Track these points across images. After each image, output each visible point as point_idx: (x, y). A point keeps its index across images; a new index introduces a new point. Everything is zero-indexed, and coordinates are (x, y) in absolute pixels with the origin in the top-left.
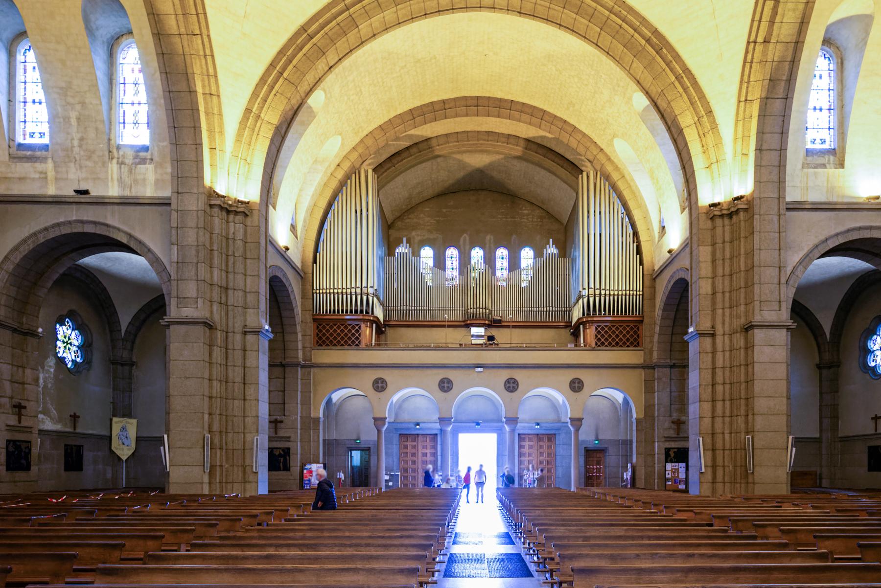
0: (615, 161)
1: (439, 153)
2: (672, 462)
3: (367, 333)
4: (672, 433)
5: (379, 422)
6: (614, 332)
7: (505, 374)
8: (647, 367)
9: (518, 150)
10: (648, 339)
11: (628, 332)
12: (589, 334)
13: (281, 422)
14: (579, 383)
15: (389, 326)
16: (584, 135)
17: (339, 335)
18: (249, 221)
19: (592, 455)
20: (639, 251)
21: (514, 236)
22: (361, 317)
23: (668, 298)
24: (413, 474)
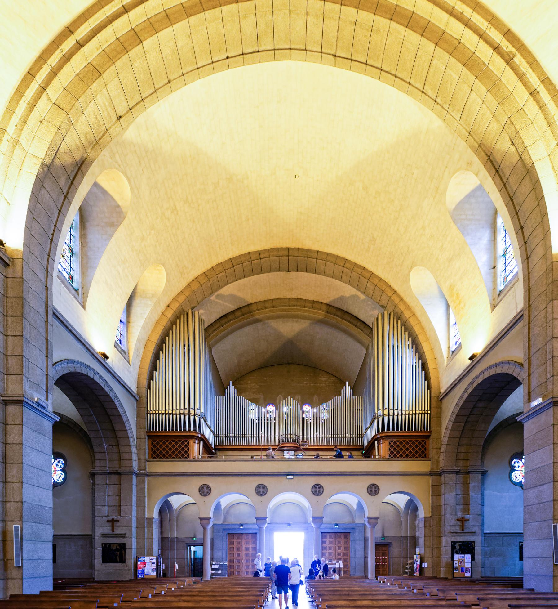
2: (457, 553)
3: (196, 448)
4: (457, 529)
5: (204, 522)
6: (404, 446)
7: (313, 481)
8: (435, 474)
9: (320, 314)
10: (435, 451)
11: (417, 446)
12: (383, 448)
13: (118, 521)
14: (375, 488)
15: (220, 450)
16: (380, 279)
17: (170, 449)
18: (10, 270)
19: (382, 547)
21: (315, 396)
23: (462, 408)
24: (238, 564)
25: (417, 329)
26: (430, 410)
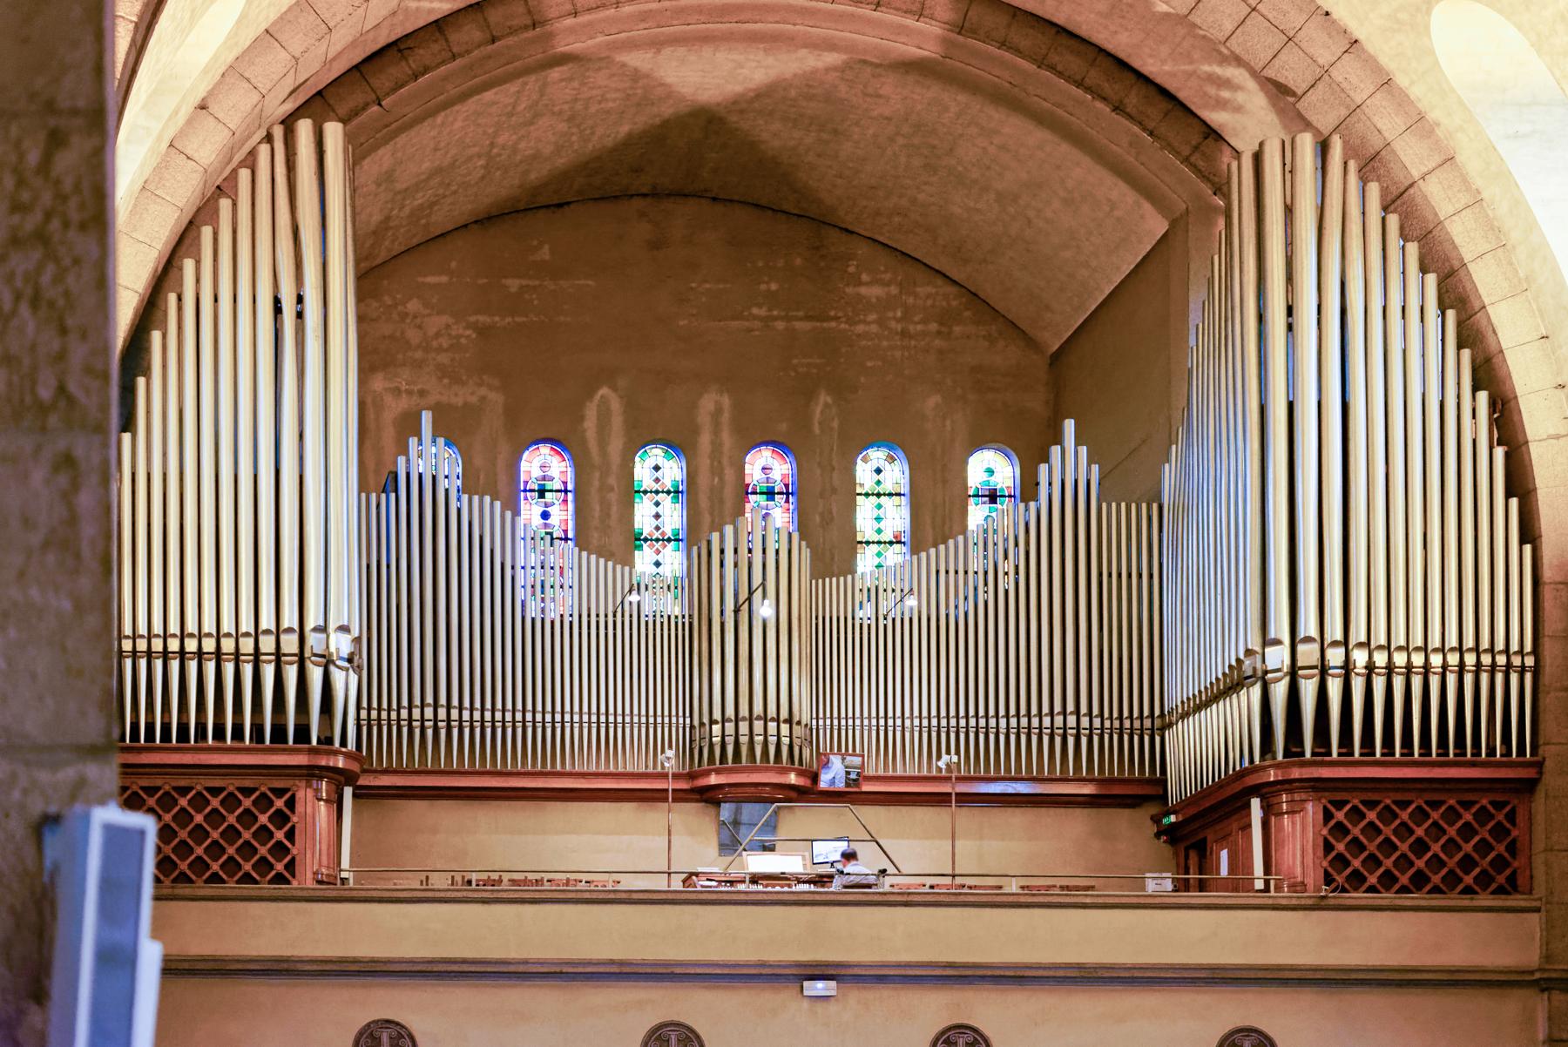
0: (1416, 92)
1: (577, 47)
17: (199, 833)
20: (1519, 483)
21: (824, 398)
22: (301, 760)
25: (1465, 237)
26: (1535, 651)
